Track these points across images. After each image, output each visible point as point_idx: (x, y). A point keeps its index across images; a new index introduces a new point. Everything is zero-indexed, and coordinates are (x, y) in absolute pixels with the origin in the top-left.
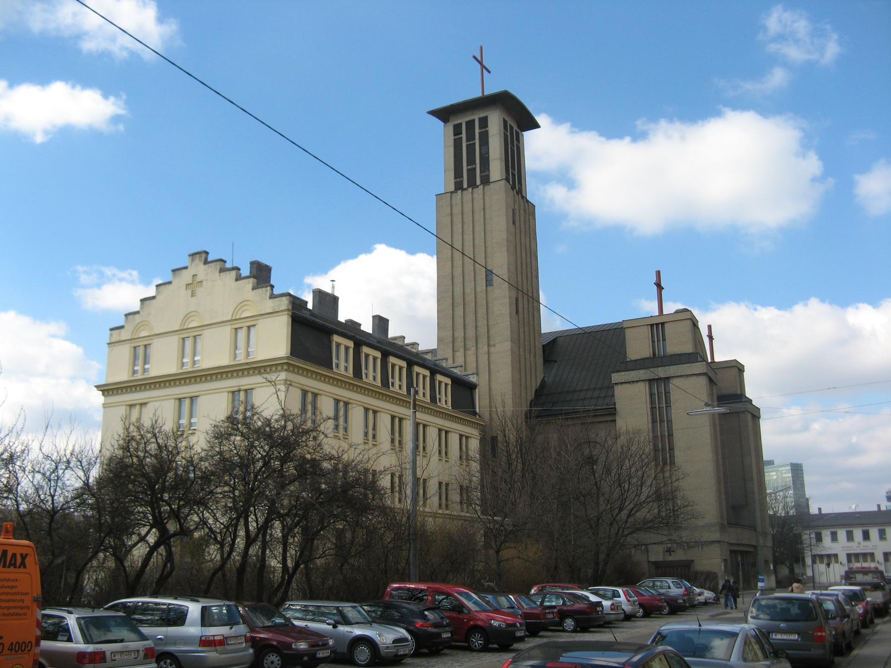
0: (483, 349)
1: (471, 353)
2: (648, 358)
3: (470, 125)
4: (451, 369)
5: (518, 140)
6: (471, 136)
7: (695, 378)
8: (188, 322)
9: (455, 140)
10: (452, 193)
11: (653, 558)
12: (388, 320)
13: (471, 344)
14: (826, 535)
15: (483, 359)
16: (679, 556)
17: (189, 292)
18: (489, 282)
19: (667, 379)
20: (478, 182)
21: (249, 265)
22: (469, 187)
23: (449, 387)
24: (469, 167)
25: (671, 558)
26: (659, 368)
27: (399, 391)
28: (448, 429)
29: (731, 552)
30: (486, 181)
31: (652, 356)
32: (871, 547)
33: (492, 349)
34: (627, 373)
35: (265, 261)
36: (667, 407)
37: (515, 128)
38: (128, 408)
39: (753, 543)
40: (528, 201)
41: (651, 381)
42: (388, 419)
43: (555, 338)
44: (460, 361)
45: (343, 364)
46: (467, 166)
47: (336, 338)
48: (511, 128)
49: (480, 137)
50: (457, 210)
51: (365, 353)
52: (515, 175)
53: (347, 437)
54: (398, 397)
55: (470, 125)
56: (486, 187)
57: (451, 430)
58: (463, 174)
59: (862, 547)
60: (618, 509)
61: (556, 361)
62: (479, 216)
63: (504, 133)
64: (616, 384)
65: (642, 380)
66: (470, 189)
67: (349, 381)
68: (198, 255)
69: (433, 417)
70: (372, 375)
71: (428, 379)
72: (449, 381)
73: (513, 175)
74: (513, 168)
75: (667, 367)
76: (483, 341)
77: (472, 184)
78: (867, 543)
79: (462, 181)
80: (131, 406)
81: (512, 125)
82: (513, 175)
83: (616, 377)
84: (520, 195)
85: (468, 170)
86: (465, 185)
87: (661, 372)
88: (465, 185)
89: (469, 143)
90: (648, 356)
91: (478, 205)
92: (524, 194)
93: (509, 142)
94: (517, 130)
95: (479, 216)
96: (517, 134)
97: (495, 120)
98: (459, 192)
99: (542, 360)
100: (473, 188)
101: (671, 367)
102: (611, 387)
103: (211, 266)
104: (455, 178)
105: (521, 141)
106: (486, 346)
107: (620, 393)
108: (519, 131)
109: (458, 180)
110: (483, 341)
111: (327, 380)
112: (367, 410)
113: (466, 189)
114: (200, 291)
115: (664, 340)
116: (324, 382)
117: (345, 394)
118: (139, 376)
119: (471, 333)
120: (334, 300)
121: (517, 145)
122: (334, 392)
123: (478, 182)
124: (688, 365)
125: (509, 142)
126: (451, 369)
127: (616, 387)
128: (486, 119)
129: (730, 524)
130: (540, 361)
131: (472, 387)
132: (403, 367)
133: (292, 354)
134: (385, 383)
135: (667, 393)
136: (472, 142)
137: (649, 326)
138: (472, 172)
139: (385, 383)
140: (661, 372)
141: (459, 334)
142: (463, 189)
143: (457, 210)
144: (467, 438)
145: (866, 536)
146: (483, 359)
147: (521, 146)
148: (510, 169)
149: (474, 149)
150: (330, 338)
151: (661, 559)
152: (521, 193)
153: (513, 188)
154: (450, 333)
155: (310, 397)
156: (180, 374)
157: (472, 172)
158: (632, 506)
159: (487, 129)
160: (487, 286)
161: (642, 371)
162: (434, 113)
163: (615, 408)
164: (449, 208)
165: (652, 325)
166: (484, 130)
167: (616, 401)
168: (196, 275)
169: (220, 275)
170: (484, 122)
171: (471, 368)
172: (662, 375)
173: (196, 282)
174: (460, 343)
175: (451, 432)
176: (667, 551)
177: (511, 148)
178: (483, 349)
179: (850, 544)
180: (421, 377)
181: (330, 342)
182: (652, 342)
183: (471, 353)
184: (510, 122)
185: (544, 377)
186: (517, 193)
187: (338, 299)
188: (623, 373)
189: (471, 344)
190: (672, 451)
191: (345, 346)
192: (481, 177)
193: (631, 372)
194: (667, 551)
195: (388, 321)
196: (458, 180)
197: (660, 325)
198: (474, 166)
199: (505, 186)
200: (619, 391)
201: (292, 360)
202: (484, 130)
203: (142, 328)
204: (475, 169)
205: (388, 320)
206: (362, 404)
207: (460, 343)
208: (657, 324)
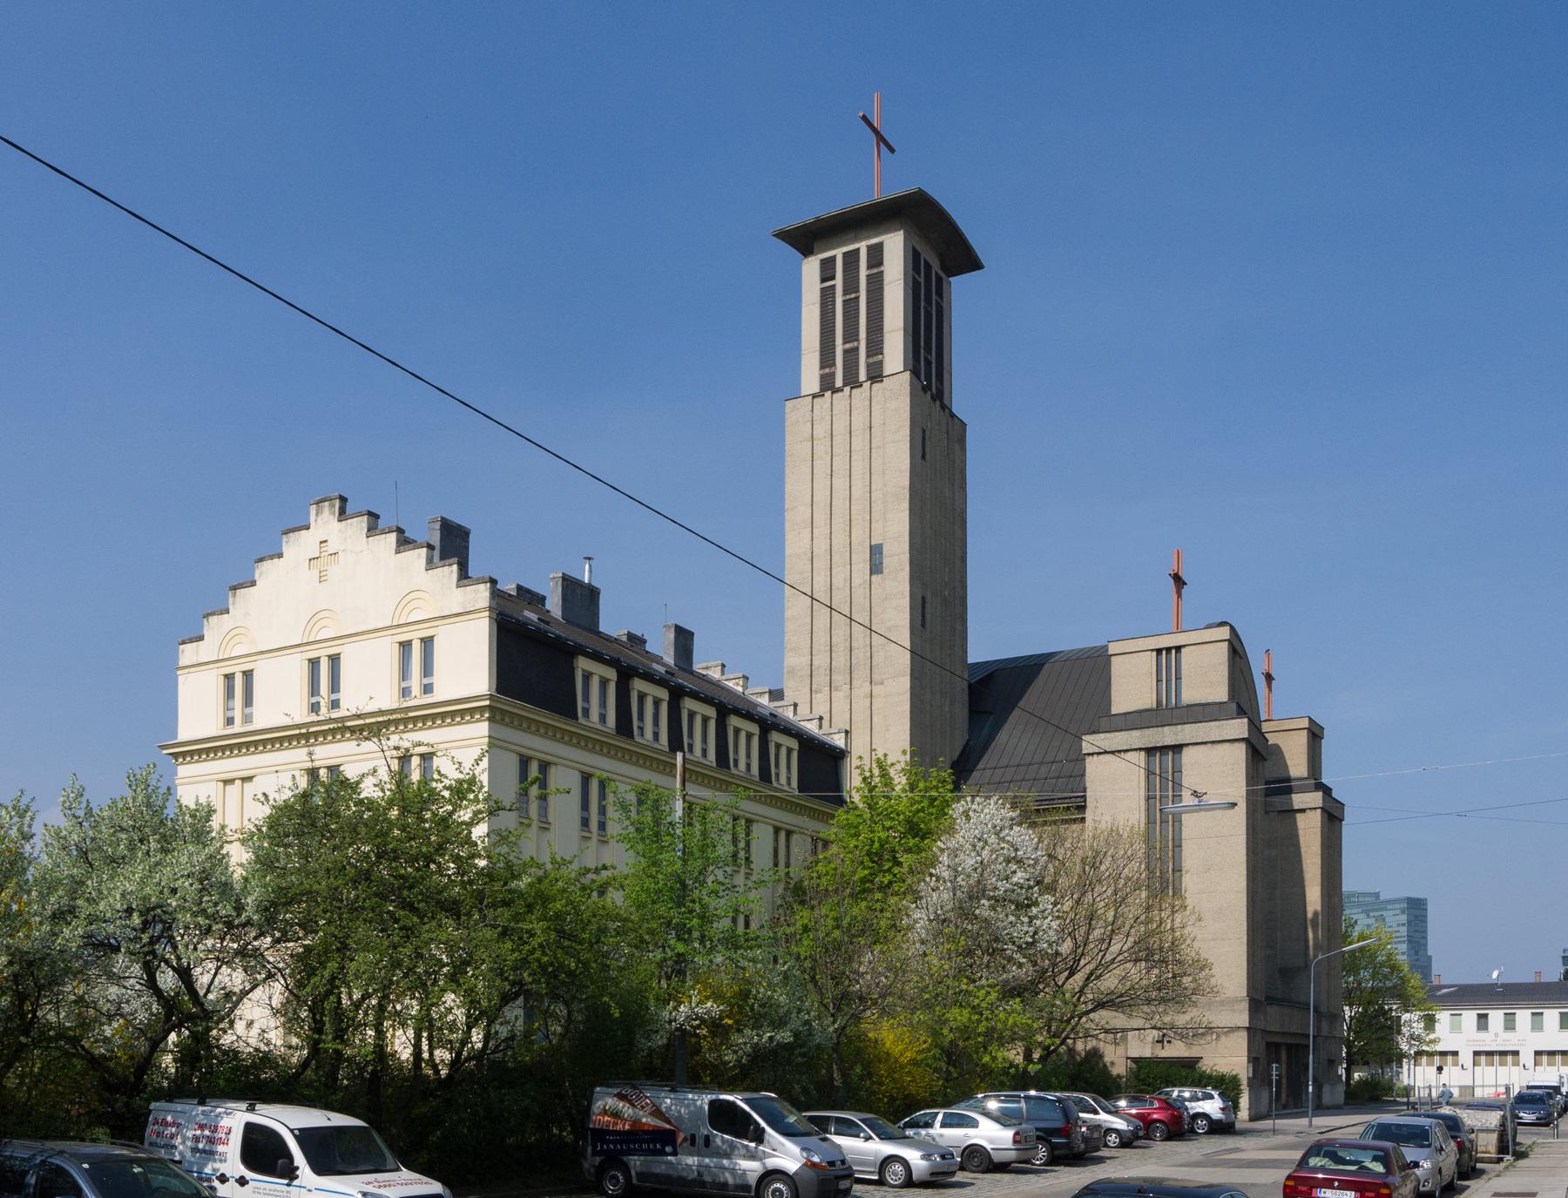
0: (862, 688)
1: (840, 697)
2: (1148, 710)
3: (851, 259)
4: (802, 723)
5: (940, 293)
6: (851, 285)
7: (1226, 745)
8: (316, 628)
9: (822, 289)
10: (814, 396)
11: (1134, 1053)
12: (692, 634)
13: (840, 678)
14: (1443, 1017)
15: (861, 705)
16: (1176, 1050)
17: (315, 573)
18: (876, 568)
19: (1177, 749)
20: (862, 376)
21: (1517, 1025)
22: (845, 385)
23: (795, 755)
24: (848, 346)
25: (1163, 1054)
26: (1166, 728)
27: (702, 760)
28: (792, 828)
29: (1269, 1045)
30: (876, 375)
31: (1154, 706)
32: (1516, 1042)
33: (877, 690)
34: (1108, 735)
35: (457, 518)
36: (1174, 796)
37: (936, 267)
38: (222, 784)
39: (1294, 1029)
40: (953, 415)
41: (1150, 751)
42: (575, 782)
43: (993, 672)
44: (841, 721)
45: (598, 709)
46: (844, 343)
47: (583, 664)
48: (928, 266)
49: (868, 283)
50: (821, 430)
51: (583, 670)
52: (931, 363)
53: (605, 839)
54: (646, 753)
55: (851, 259)
56: (876, 386)
57: (758, 818)
58: (834, 360)
59: (1499, 1040)
60: (1067, 972)
61: (991, 713)
62: (859, 443)
63: (914, 278)
64: (1089, 754)
65: (1136, 750)
66: (847, 389)
67: (664, 758)
68: (327, 503)
69: (785, 813)
70: (652, 730)
71: (755, 741)
72: (794, 744)
73: (928, 363)
74: (851, 334)
75: (1179, 727)
76: (861, 673)
77: (852, 381)
78: (1509, 1035)
79: (833, 374)
80: (226, 782)
81: (931, 262)
82: (928, 363)
83: (1089, 743)
84: (938, 402)
85: (846, 352)
86: (839, 383)
87: (1168, 736)
88: (839, 383)
89: (848, 297)
90: (1148, 706)
91: (859, 421)
92: (945, 402)
93: (923, 297)
94: (940, 272)
95: (859, 443)
96: (939, 280)
97: (894, 245)
98: (828, 394)
99: (966, 712)
100: (852, 388)
101: (1187, 726)
102: (1080, 759)
103: (351, 524)
104: (822, 367)
105: (911, 253)
106: (868, 683)
107: (1095, 769)
108: (943, 275)
109: (827, 370)
110: (861, 673)
111: (634, 759)
112: (777, 830)
113: (840, 390)
114: (334, 571)
115: (1178, 678)
116: (622, 759)
117: (601, 764)
118: (238, 728)
119: (841, 660)
120: (592, 594)
121: (938, 303)
122: (581, 760)
123: (862, 376)
124: (1217, 723)
125: (923, 297)
126: (802, 723)
127: (1089, 760)
128: (880, 246)
129: (1271, 1000)
130: (962, 713)
131: (836, 757)
132: (661, 700)
133: (498, 690)
134: (624, 726)
135: (1177, 770)
136: (853, 296)
137: (1155, 653)
138: (851, 355)
139: (624, 726)
140: (1168, 736)
141: (821, 660)
142: (835, 391)
143: (821, 430)
144: (749, 822)
145: (1510, 1024)
146: (861, 705)
147: (911, 272)
148: (922, 351)
149: (857, 310)
150: (572, 663)
151: (1147, 1053)
152: (941, 401)
153: (925, 389)
154: (806, 660)
155: (534, 771)
156: (313, 724)
157: (851, 355)
158: (1092, 966)
159: (882, 268)
160: (871, 575)
161: (1136, 733)
162: (785, 236)
163: (1084, 796)
164: (809, 425)
165: (1159, 651)
166: (875, 271)
167: (1087, 785)
168: (326, 541)
169: (368, 542)
170: (876, 256)
171: (841, 721)
172: (1169, 741)
173: (326, 554)
174: (821, 679)
175: (757, 821)
176: (1158, 1042)
177: (925, 307)
178: (862, 688)
179: (1482, 1035)
180: (743, 736)
181: (572, 670)
182: (1158, 681)
183: (840, 697)
184: (928, 255)
185: (969, 740)
186: (933, 399)
187: (599, 593)
188: (1102, 736)
189: (840, 678)
190: (1177, 874)
191: (654, 697)
192: (868, 366)
193: (1117, 734)
194: (1158, 1042)
195: (692, 634)
196: (827, 370)
197: (1173, 651)
198: (856, 344)
199: (912, 384)
200: (1092, 765)
201: (538, 715)
202: (875, 271)
203: (236, 639)
204: (856, 349)
205: (692, 634)
206: (578, 766)
207: (821, 679)
208: (1168, 650)
